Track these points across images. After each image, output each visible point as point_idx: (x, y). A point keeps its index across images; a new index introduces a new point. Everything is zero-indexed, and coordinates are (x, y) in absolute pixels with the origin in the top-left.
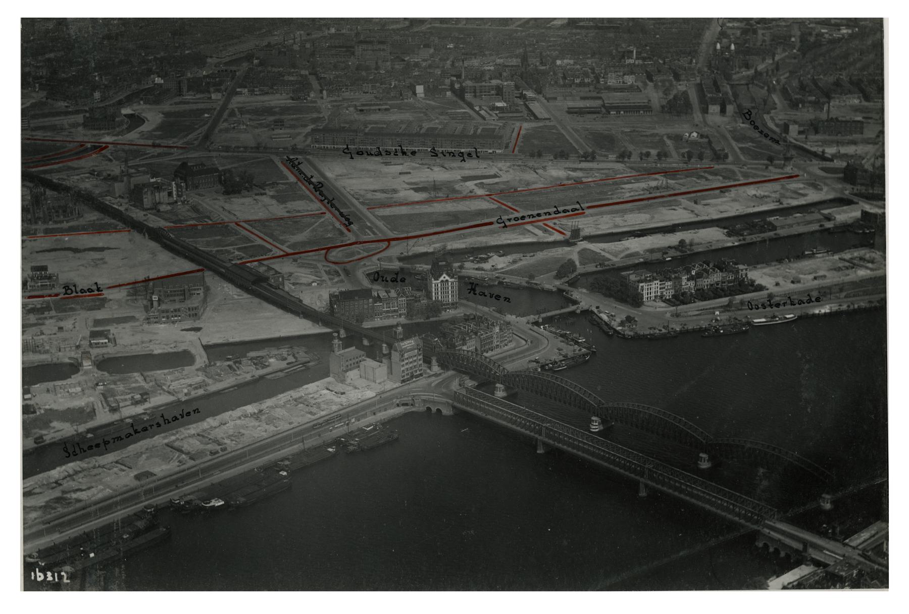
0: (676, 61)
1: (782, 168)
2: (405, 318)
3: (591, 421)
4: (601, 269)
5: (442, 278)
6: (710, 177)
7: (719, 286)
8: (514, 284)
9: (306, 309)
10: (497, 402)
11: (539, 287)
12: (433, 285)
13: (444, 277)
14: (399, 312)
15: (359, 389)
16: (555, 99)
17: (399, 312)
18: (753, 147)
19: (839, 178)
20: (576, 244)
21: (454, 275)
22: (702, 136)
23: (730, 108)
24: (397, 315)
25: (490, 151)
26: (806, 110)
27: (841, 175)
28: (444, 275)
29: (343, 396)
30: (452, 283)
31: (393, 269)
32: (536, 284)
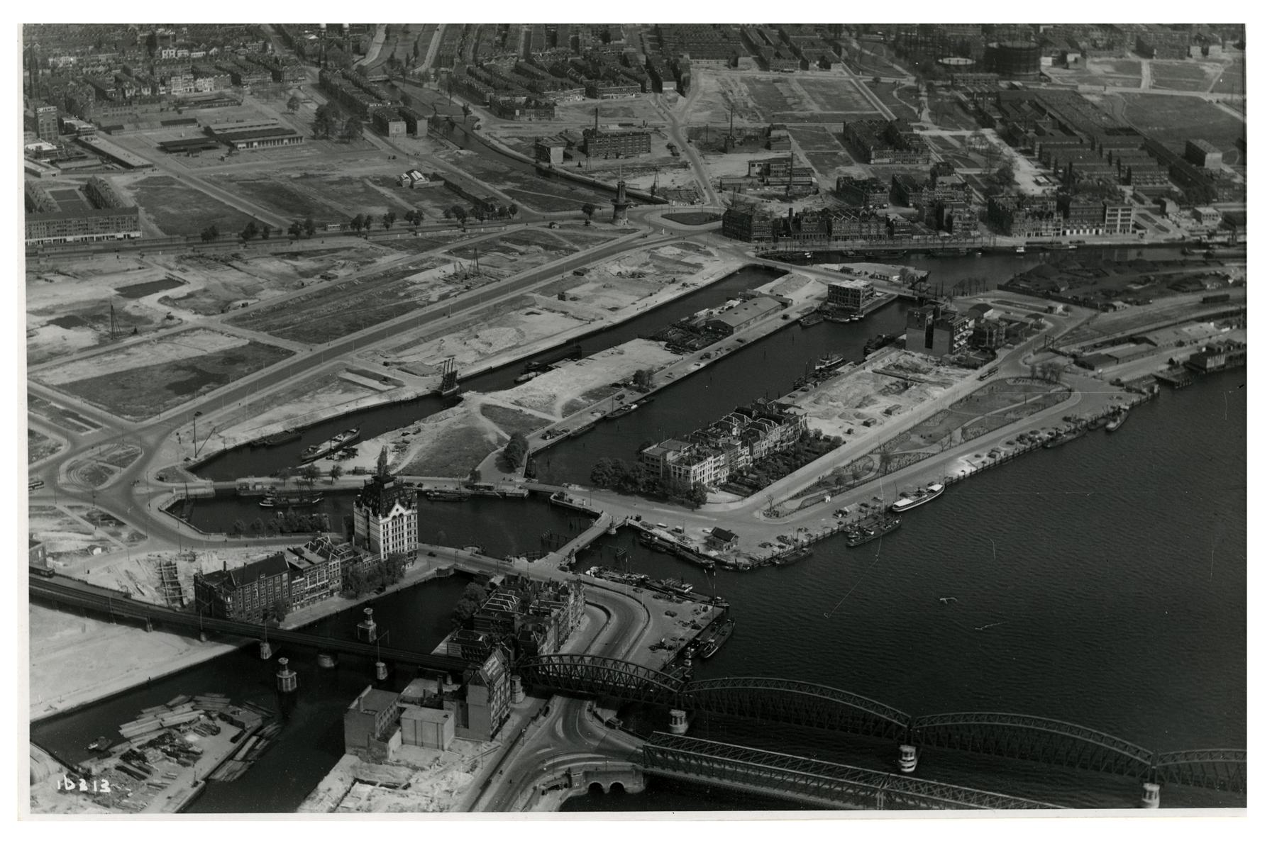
0: (242, 49)
1: (611, 222)
2: (339, 596)
3: (900, 754)
4: (553, 441)
5: (393, 513)
6: (522, 249)
7: (778, 449)
8: (445, 492)
9: (154, 611)
10: (678, 742)
11: (495, 492)
12: (381, 527)
13: (398, 509)
14: (331, 587)
15: (423, 769)
16: (121, 127)
17: (331, 587)
18: (520, 188)
19: (715, 231)
20: (461, 400)
21: (410, 502)
22: (435, 177)
23: (422, 125)
24: (327, 594)
25: (120, 235)
26: (526, 119)
27: (719, 224)
28: (397, 506)
29: (409, 791)
30: (409, 518)
31: (205, 495)
32: (489, 488)
